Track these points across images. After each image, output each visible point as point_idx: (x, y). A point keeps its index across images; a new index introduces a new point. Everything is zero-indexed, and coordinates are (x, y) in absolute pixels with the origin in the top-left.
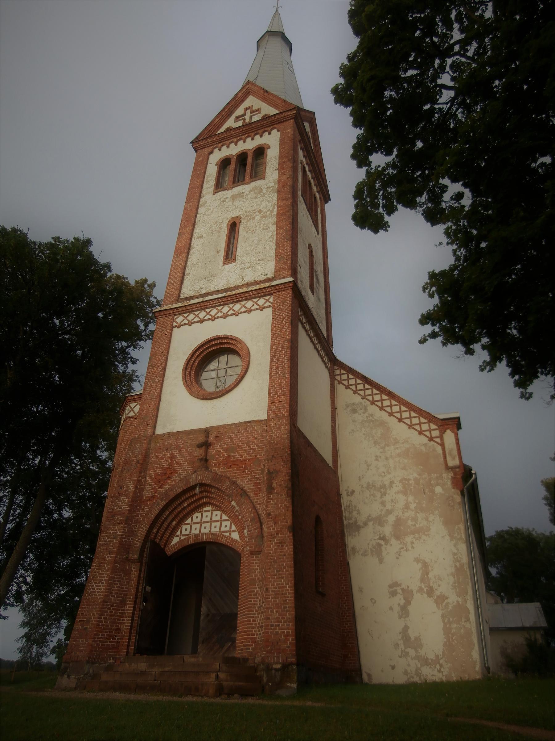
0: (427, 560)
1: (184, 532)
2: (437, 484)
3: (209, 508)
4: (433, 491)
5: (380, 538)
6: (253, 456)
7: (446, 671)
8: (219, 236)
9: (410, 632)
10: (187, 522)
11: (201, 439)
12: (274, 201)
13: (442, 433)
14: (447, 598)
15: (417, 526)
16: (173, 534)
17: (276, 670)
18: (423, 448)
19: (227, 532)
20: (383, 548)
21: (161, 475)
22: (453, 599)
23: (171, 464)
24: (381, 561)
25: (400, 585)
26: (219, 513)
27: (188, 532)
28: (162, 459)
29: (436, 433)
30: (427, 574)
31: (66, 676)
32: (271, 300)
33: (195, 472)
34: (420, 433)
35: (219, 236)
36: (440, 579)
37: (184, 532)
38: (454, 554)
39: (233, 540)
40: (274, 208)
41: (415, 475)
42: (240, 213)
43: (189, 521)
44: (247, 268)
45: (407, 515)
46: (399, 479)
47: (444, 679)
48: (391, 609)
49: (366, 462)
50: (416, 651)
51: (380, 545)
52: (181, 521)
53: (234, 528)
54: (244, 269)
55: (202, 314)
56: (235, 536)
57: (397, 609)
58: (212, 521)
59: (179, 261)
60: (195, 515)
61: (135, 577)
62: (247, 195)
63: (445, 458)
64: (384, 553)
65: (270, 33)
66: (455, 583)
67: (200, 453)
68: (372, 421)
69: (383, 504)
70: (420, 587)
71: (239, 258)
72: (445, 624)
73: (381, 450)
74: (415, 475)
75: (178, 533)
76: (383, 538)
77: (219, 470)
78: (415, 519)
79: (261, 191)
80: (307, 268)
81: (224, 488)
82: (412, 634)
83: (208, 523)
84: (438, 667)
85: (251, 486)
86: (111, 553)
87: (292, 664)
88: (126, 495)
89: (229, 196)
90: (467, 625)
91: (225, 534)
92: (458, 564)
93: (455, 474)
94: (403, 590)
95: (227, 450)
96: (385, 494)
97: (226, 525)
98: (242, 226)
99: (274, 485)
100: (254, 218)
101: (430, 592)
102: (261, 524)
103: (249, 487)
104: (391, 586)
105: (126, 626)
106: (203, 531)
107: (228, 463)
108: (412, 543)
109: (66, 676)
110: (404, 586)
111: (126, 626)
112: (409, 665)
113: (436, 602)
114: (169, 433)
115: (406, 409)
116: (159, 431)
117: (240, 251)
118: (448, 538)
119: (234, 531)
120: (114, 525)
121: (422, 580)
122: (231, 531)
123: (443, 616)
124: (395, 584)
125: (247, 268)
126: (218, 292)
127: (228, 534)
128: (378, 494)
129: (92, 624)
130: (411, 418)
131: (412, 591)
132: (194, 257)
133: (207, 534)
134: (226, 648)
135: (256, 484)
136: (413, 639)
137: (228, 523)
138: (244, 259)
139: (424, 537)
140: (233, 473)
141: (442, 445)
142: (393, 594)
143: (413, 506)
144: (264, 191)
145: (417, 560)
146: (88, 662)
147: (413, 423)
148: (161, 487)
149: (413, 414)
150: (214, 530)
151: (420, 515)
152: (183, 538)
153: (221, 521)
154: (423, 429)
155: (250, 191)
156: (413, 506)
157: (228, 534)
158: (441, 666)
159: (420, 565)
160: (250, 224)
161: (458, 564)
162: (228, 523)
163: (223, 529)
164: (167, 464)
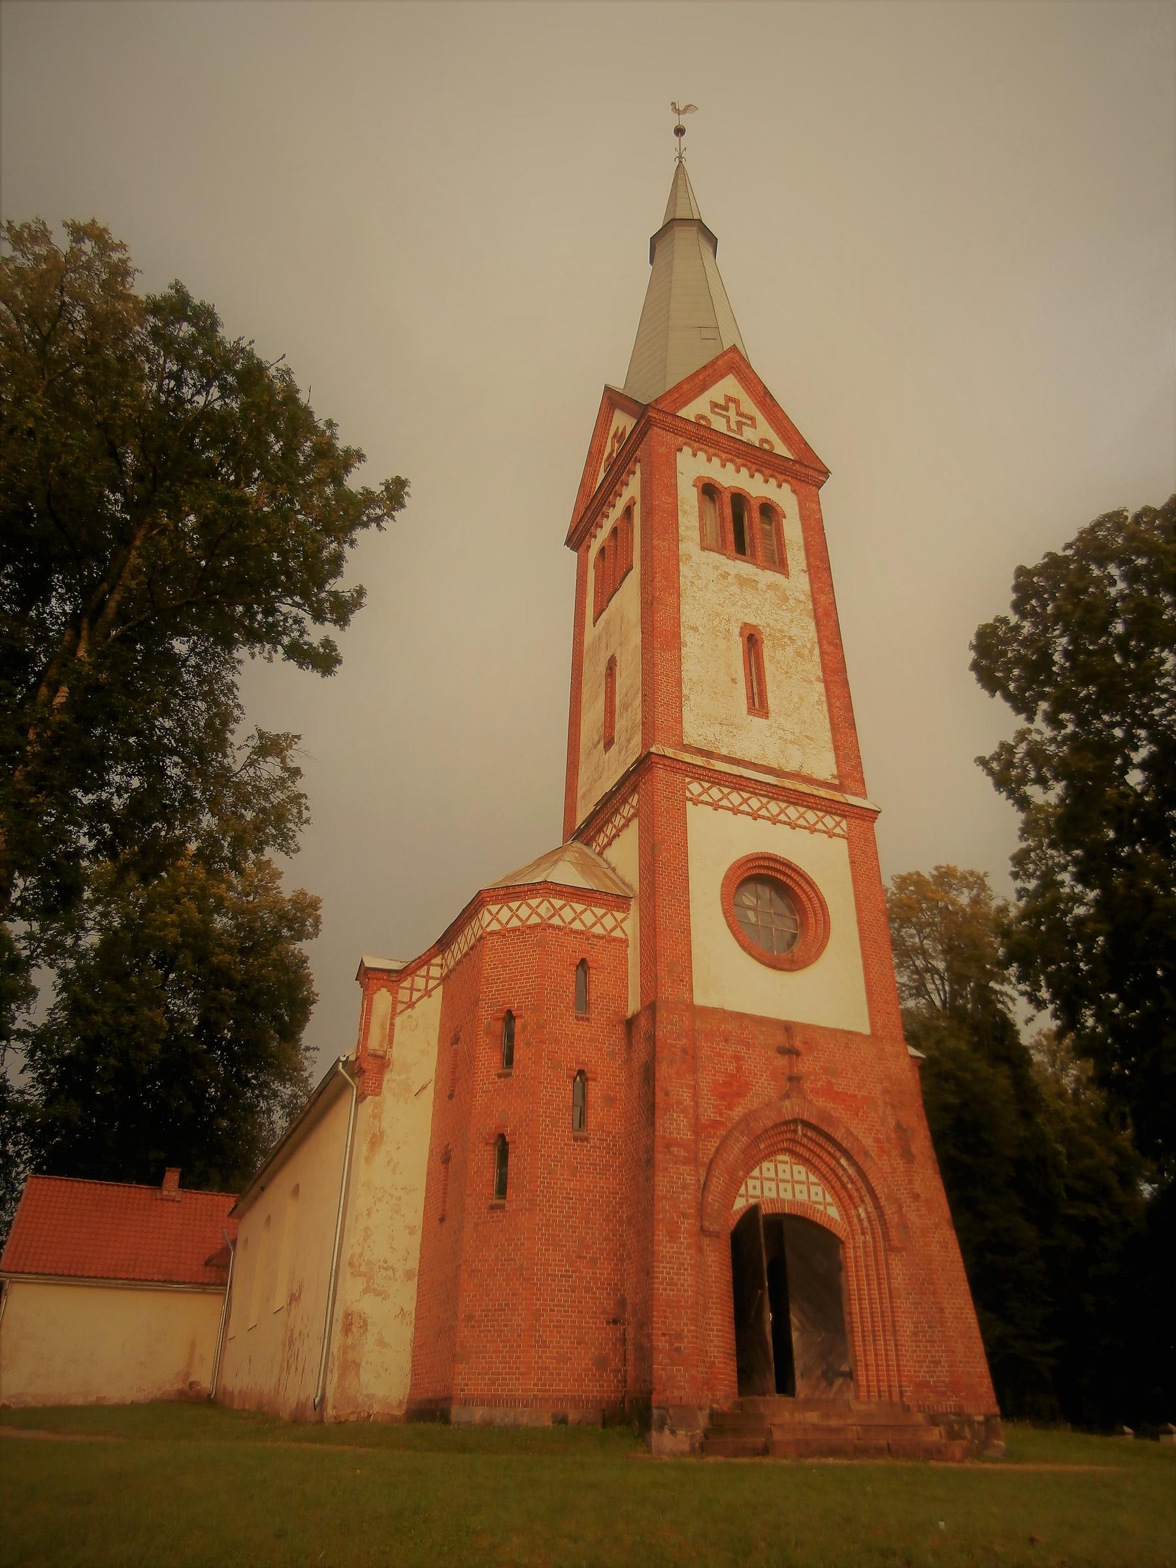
1: (820, 1198)
17: (979, 1423)
19: (820, 1203)
23: (739, 1068)
28: (719, 1055)
31: (667, 1432)
39: (830, 1219)
43: (813, 1179)
44: (791, 742)
53: (829, 1199)
56: (833, 1212)
61: (713, 1261)
65: (671, 224)
67: (781, 1062)
77: (820, 1102)
80: (601, 703)
86: (685, 1216)
87: (995, 1415)
88: (683, 1111)
89: (733, 572)
91: (818, 1206)
99: (914, 1150)
100: (784, 648)
102: (900, 1207)
105: (715, 1346)
106: (783, 1195)
107: (829, 1092)
109: (667, 1432)
111: (715, 1346)
116: (866, 1030)
120: (676, 1163)
122: (826, 1205)
125: (791, 742)
129: (689, 1342)
133: (790, 1202)
135: (877, 1140)
138: (781, 719)
144: (792, 601)
148: (730, 1107)
154: (406, 999)
155: (769, 587)
163: (813, 1198)
164: (731, 1068)
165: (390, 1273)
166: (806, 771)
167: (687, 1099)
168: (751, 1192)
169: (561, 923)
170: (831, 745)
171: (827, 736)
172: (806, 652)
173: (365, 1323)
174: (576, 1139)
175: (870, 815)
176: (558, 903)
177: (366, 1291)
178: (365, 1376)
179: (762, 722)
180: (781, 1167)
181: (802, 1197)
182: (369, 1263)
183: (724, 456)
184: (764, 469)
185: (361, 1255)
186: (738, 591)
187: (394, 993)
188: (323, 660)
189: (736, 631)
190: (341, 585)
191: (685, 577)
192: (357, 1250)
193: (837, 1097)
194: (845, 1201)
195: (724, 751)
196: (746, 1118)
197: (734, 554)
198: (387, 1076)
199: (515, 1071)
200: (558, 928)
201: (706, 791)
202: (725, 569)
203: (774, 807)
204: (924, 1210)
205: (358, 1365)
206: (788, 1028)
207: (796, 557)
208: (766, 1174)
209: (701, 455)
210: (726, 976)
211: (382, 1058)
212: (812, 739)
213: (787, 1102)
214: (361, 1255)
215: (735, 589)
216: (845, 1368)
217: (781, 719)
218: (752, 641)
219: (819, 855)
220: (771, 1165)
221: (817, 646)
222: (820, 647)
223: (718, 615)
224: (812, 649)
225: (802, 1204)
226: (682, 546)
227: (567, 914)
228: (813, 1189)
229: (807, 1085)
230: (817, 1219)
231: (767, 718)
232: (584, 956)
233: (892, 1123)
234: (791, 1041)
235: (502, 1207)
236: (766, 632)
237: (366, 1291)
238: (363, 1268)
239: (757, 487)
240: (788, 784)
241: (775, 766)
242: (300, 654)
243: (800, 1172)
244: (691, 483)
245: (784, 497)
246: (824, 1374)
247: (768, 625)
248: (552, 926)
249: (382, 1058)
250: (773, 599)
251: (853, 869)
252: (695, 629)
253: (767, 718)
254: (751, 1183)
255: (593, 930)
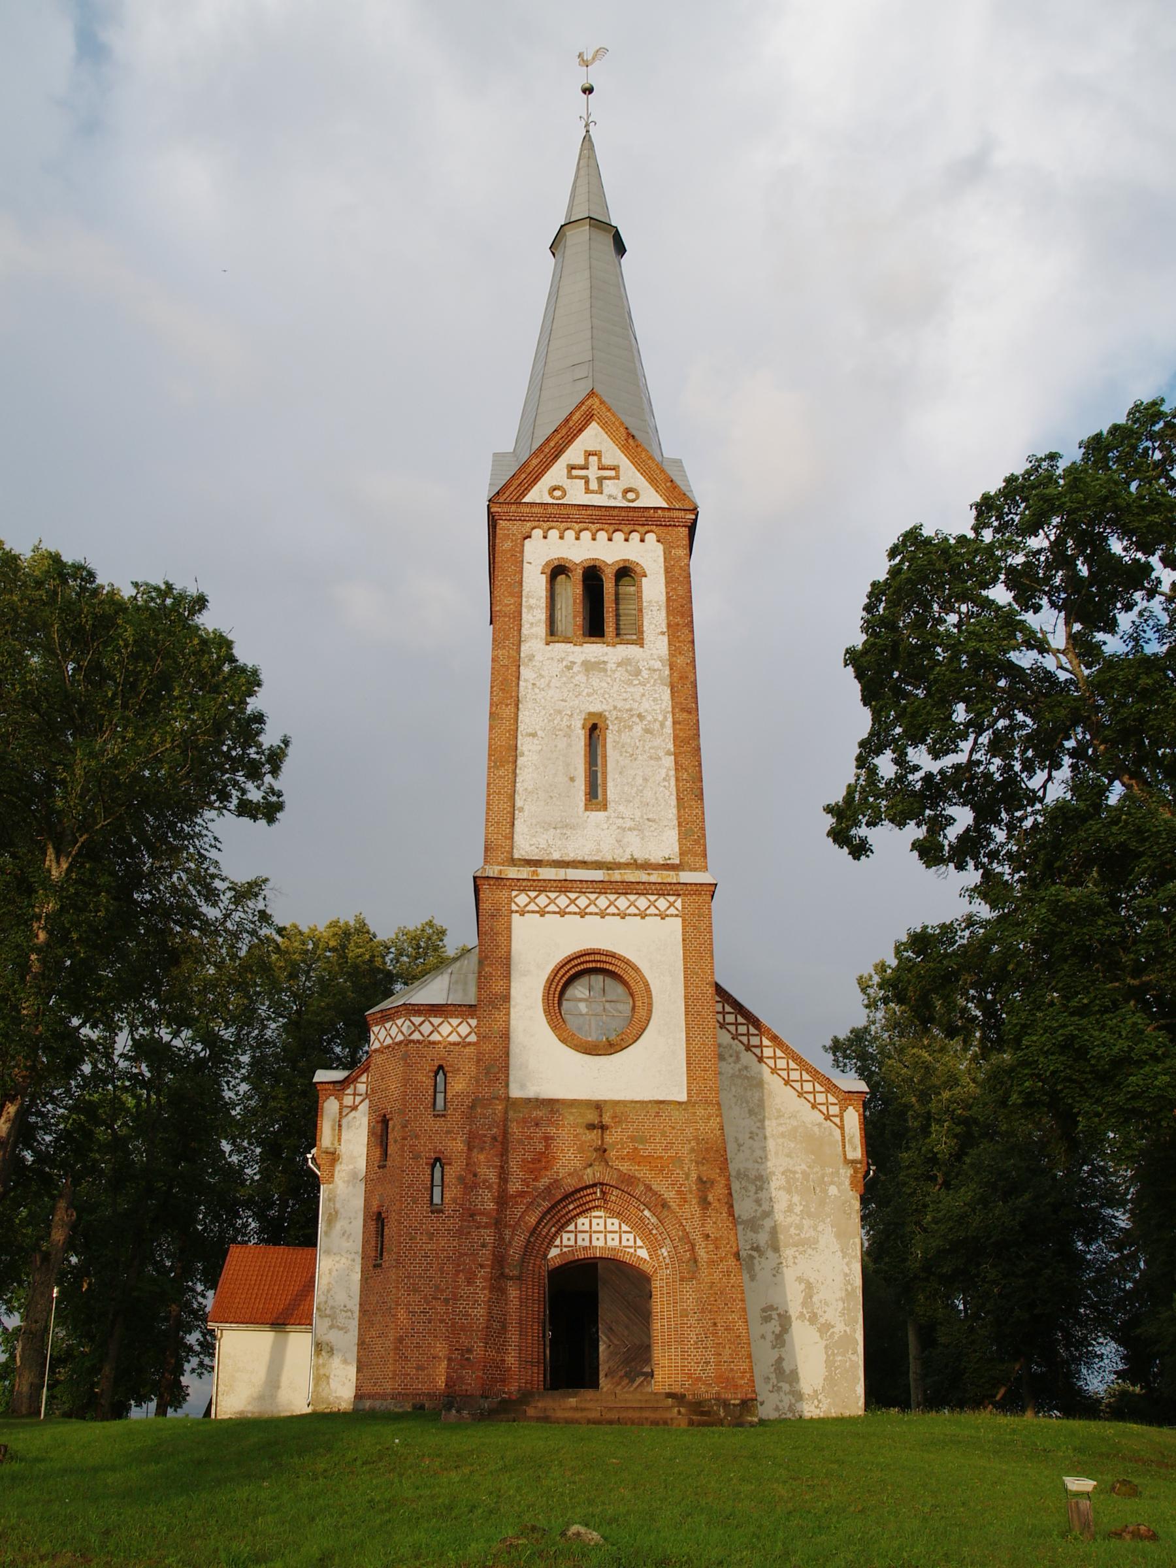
0: (811, 1280)
1: (631, 1243)
2: (832, 1183)
3: (601, 1214)
4: (825, 1191)
5: (752, 1249)
6: (672, 1153)
7: (824, 1407)
8: (570, 745)
9: (785, 1364)
10: (569, 1228)
11: (592, 1117)
12: (665, 704)
13: (843, 1110)
14: (833, 1327)
15: (802, 1236)
16: (550, 1244)
18: (816, 1129)
20: (756, 1261)
21: (533, 1161)
22: (840, 1327)
24: (753, 1278)
25: (777, 1309)
26: (616, 1221)
27: (572, 1243)
29: (834, 1110)
30: (811, 1297)
32: (679, 904)
33: (591, 1165)
34: (814, 1106)
35: (570, 745)
36: (826, 1304)
37: (565, 1242)
38: (846, 1275)
40: (665, 718)
41: (804, 1167)
42: (605, 707)
43: (571, 1227)
44: (630, 829)
45: (789, 1220)
46: (782, 1169)
47: (822, 1415)
48: (763, 1337)
49: (736, 1139)
50: (791, 1385)
51: (752, 1257)
52: (561, 1228)
53: (639, 1243)
54: (624, 829)
55: (563, 901)
56: (643, 1253)
57: (770, 1337)
58: (606, 1232)
59: (500, 777)
60: (580, 1220)
62: (614, 671)
63: (844, 1147)
64: (757, 1268)
66: (844, 1309)
67: (593, 1136)
68: (747, 1078)
69: (758, 1202)
70: (802, 1313)
71: (613, 804)
72: (828, 1356)
73: (758, 1124)
74: (804, 1167)
75: (557, 1242)
76: (757, 1249)
77: (625, 1167)
78: (800, 1227)
79: (638, 673)
81: (637, 1192)
82: (787, 1367)
83: (600, 1233)
84: (816, 1402)
85: (672, 1194)
86: (482, 1266)
90: (854, 1358)
92: (849, 1288)
93: (856, 1171)
94: (779, 1315)
95: (633, 1139)
96: (761, 1188)
97: (629, 1239)
98: (611, 737)
99: (710, 1198)
100: (631, 728)
101: (813, 1319)
102: (693, 1246)
103: (670, 1195)
104: (764, 1310)
106: (595, 1243)
107: (634, 1157)
108: (795, 1257)
110: (781, 1311)
112: (781, 1401)
113: (819, 1330)
114: (529, 1100)
115: (796, 1067)
117: (612, 791)
118: (839, 1254)
119: (641, 1247)
121: (804, 1304)
122: (636, 1248)
123: (826, 1347)
124: (771, 1308)
125: (630, 829)
126: (584, 864)
127: (632, 1250)
128: (752, 1188)
130: (788, 1069)
131: (790, 1317)
132: (527, 777)
133: (601, 1248)
134: (637, 1383)
135: (679, 1192)
136: (788, 1372)
137: (631, 1236)
138: (621, 808)
139: (810, 1251)
140: (643, 1172)
141: (842, 1128)
142: (767, 1319)
143: (798, 1209)
144: (645, 674)
145: (800, 1279)
146: (482, 1396)
147: (805, 1089)
149: (806, 1076)
150: (610, 1243)
151: (807, 1223)
152: (565, 1250)
153: (620, 1232)
155: (619, 665)
156: (798, 1209)
157: (632, 1250)
158: (819, 1401)
159: (803, 1286)
160: (625, 737)
161: (849, 1288)
162: (631, 1236)
163: (624, 1243)
164: (541, 1147)
165: (349, 1314)
166: (641, 856)
167: (492, 1176)
168: (565, 1242)
169: (421, 1038)
170: (676, 822)
171: (672, 813)
172: (657, 726)
173: (332, 1349)
174: (432, 1212)
175: (711, 889)
176: (417, 1020)
177: (331, 1327)
178: (334, 1384)
179: (601, 815)
180: (595, 1221)
181: (613, 1242)
182: (332, 1308)
183: (577, 526)
184: (621, 527)
185: (326, 1302)
186: (584, 679)
187: (340, 1099)
188: (270, 810)
189: (579, 724)
190: (269, 738)
191: (526, 681)
192: (323, 1298)
193: (648, 1160)
194: (653, 1246)
195: (556, 856)
196: (548, 1189)
197: (581, 639)
198: (338, 1168)
199: (389, 1163)
200: (418, 1041)
201: (533, 900)
202: (571, 658)
203: (603, 902)
204: (711, 1247)
205: (328, 1377)
206: (598, 1106)
207: (655, 620)
208: (580, 1228)
209: (554, 534)
210: (547, 1066)
211: (333, 1153)
212: (654, 821)
213: (589, 1170)
214: (326, 1302)
215: (581, 678)
216: (647, 1369)
217: (621, 808)
218: (594, 730)
219: (649, 941)
220: (587, 1221)
221: (670, 716)
222: (673, 714)
223: (560, 712)
224: (665, 718)
225: (613, 1249)
226: (524, 648)
227: (426, 1028)
228: (625, 1236)
229: (612, 1154)
230: (627, 1259)
231: (605, 809)
232: (441, 1062)
233: (694, 1176)
234: (600, 1117)
235: (380, 1265)
236: (611, 716)
237: (331, 1327)
238: (328, 1312)
239: (608, 550)
240: (617, 876)
241: (609, 858)
242: (246, 809)
243: (614, 1223)
244: (540, 569)
245: (647, 552)
246: (626, 1375)
247: (615, 708)
248: (413, 1041)
249: (333, 1153)
250: (625, 678)
251: (684, 947)
252: (534, 735)
253: (605, 809)
254: (565, 1236)
255: (449, 1039)
